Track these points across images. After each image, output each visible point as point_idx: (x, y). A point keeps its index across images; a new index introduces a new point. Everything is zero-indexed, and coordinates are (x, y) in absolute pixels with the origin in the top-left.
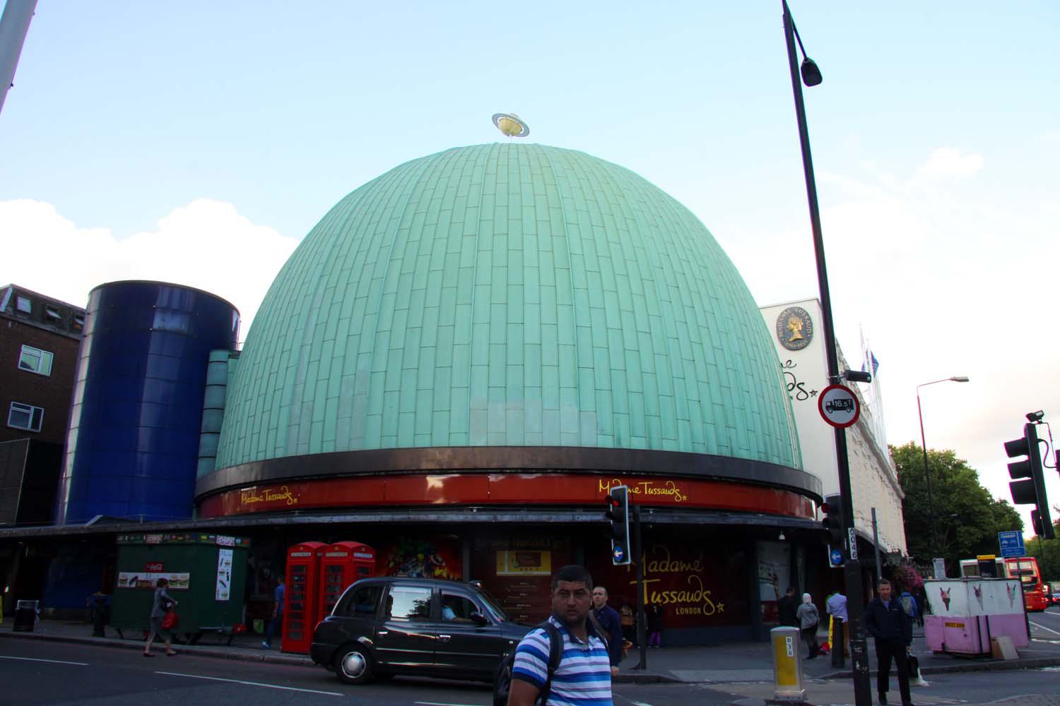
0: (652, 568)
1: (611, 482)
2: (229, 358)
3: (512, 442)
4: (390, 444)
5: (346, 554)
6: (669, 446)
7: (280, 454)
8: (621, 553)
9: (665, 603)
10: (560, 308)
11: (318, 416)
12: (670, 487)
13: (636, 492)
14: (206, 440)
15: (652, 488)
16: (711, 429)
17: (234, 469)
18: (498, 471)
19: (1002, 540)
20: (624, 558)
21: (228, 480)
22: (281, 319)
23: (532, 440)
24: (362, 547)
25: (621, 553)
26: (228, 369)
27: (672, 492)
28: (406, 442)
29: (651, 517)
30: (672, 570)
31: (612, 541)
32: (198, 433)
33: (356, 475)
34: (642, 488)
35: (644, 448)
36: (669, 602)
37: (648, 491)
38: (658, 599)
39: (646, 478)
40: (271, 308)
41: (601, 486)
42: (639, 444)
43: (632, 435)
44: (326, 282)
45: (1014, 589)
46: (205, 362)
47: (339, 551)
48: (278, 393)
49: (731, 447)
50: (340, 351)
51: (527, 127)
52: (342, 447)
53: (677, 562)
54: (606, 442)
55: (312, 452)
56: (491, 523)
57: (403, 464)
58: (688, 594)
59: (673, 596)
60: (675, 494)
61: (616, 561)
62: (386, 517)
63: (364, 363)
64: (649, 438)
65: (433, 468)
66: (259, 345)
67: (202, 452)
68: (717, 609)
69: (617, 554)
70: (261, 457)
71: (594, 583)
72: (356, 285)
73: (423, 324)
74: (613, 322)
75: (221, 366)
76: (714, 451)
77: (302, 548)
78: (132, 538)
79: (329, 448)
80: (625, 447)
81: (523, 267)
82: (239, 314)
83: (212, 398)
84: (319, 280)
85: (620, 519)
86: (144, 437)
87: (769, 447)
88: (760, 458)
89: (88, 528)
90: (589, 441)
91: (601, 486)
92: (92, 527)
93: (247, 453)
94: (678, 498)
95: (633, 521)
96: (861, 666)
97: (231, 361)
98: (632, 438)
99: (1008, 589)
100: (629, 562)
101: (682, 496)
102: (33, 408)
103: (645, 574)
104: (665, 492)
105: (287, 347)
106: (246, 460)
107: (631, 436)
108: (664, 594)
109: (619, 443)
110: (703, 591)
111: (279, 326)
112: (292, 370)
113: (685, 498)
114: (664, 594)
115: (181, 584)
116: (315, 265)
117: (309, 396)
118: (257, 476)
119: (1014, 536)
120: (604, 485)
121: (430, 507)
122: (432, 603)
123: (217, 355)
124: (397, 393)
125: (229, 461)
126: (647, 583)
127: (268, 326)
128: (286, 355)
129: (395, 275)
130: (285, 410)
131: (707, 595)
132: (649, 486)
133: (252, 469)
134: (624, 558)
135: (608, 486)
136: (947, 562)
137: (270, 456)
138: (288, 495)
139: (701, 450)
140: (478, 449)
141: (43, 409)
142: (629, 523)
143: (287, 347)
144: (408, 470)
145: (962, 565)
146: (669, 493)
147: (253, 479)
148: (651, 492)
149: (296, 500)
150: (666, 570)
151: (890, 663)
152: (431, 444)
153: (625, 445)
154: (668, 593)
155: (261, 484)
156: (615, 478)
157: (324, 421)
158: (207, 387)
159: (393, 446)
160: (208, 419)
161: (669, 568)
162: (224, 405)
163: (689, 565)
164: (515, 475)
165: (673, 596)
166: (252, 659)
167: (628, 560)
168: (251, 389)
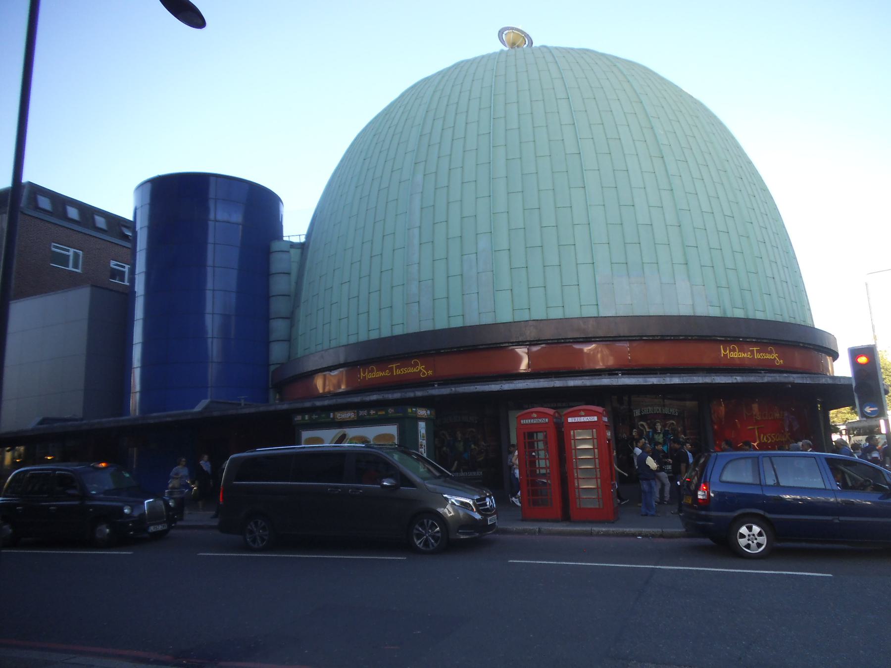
2: (291, 248)
5: (595, 419)
6: (760, 316)
9: (769, 442)
12: (771, 352)
13: (387, 374)
15: (400, 369)
18: (601, 339)
33: (498, 345)
34: (391, 370)
36: (771, 442)
39: (756, 344)
42: (739, 314)
47: (537, 418)
51: (530, 38)
53: (740, 353)
54: (715, 312)
59: (773, 437)
60: (421, 371)
62: (739, 379)
63: (483, 243)
64: (744, 308)
68: (428, 374)
71: (879, 434)
75: (285, 256)
78: (314, 417)
79: (413, 328)
80: (729, 316)
81: (624, 155)
82: (283, 204)
86: (212, 323)
89: (200, 413)
90: (702, 310)
91: (362, 374)
94: (424, 374)
101: (427, 371)
102: (72, 250)
104: (411, 370)
107: (733, 308)
108: (767, 436)
120: (725, 350)
129: (419, 177)
132: (397, 367)
135: (728, 351)
137: (363, 337)
139: (779, 319)
140: (619, 318)
141: (81, 252)
146: (415, 370)
147: (342, 361)
148: (398, 372)
150: (737, 356)
152: (464, 323)
153: (729, 315)
154: (769, 434)
155: (351, 366)
156: (413, 359)
163: (746, 354)
165: (773, 437)
166: (598, 534)
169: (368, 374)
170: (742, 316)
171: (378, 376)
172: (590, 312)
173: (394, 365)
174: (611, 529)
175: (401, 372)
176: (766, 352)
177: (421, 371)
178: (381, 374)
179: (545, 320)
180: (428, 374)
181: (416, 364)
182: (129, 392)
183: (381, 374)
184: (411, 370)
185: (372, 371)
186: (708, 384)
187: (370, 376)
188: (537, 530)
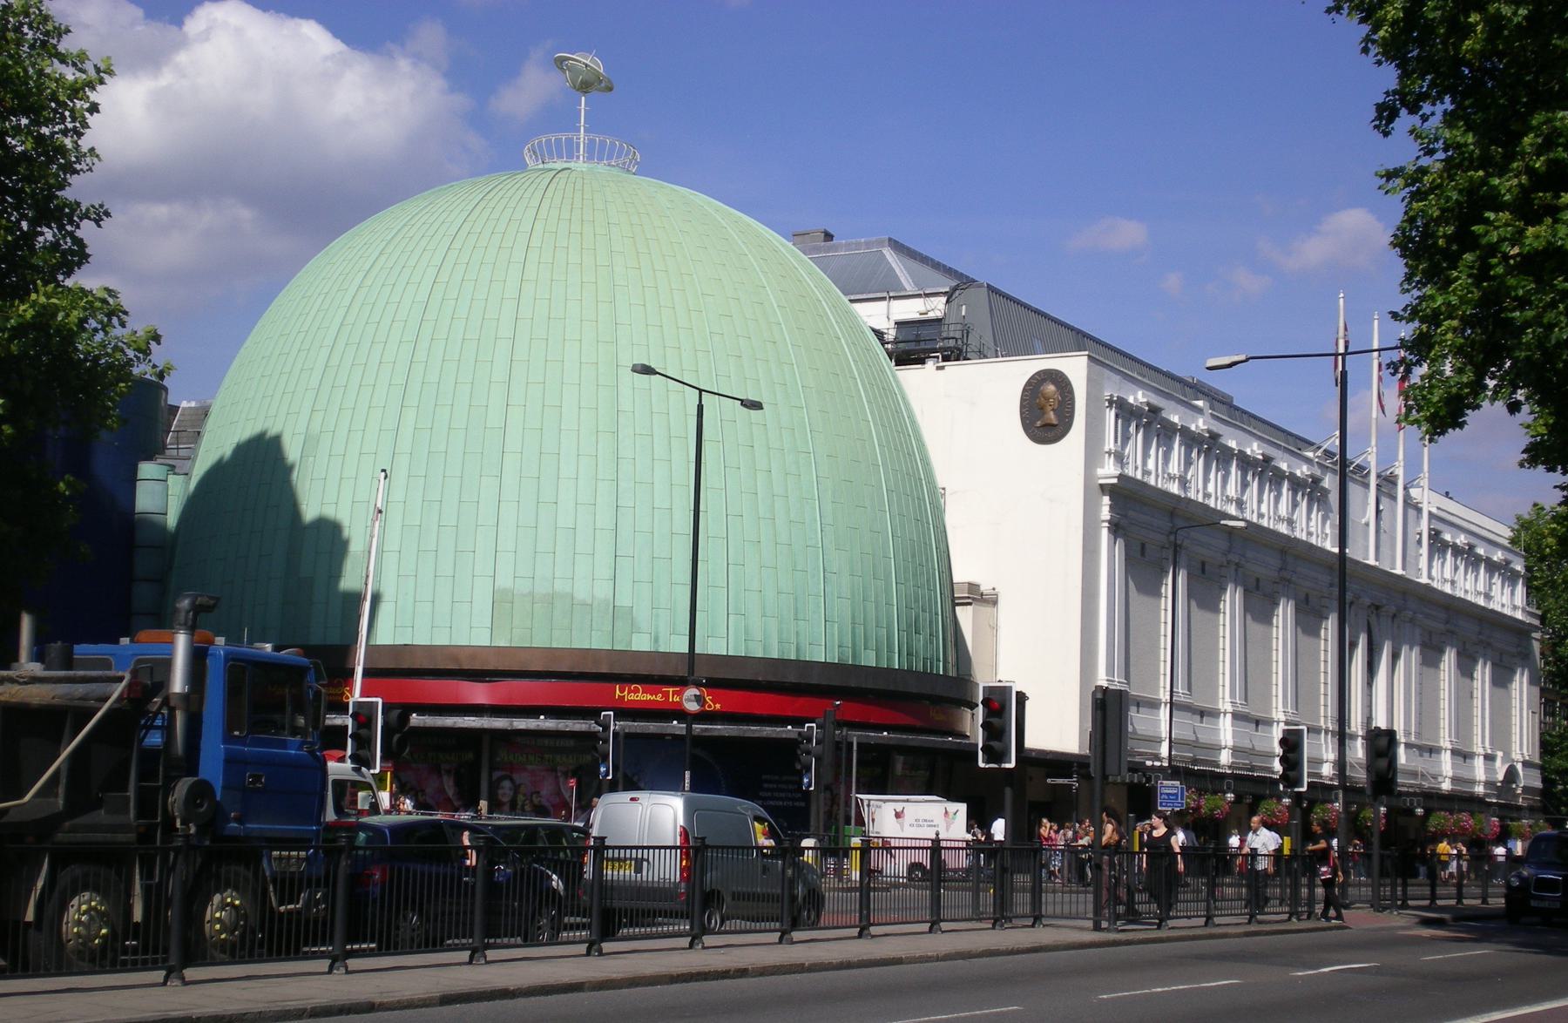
1: (629, 688)
16: (871, 607)
19: (1161, 794)
28: (422, 639)
34: (666, 695)
37: (673, 698)
38: (678, 699)
44: (322, 316)
45: (955, 814)
49: (797, 644)
56: (507, 730)
91: (618, 692)
92: (116, 706)
99: (946, 812)
115: (1510, 177)
116: (311, 313)
119: (1176, 791)
120: (622, 691)
121: (770, 823)
122: (421, 798)
135: (626, 693)
136: (881, 784)
145: (326, 679)
149: (718, 706)
164: (1335, 604)
173: (671, 690)
178: (649, 697)
183: (649, 697)
185: (636, 691)
187: (632, 697)
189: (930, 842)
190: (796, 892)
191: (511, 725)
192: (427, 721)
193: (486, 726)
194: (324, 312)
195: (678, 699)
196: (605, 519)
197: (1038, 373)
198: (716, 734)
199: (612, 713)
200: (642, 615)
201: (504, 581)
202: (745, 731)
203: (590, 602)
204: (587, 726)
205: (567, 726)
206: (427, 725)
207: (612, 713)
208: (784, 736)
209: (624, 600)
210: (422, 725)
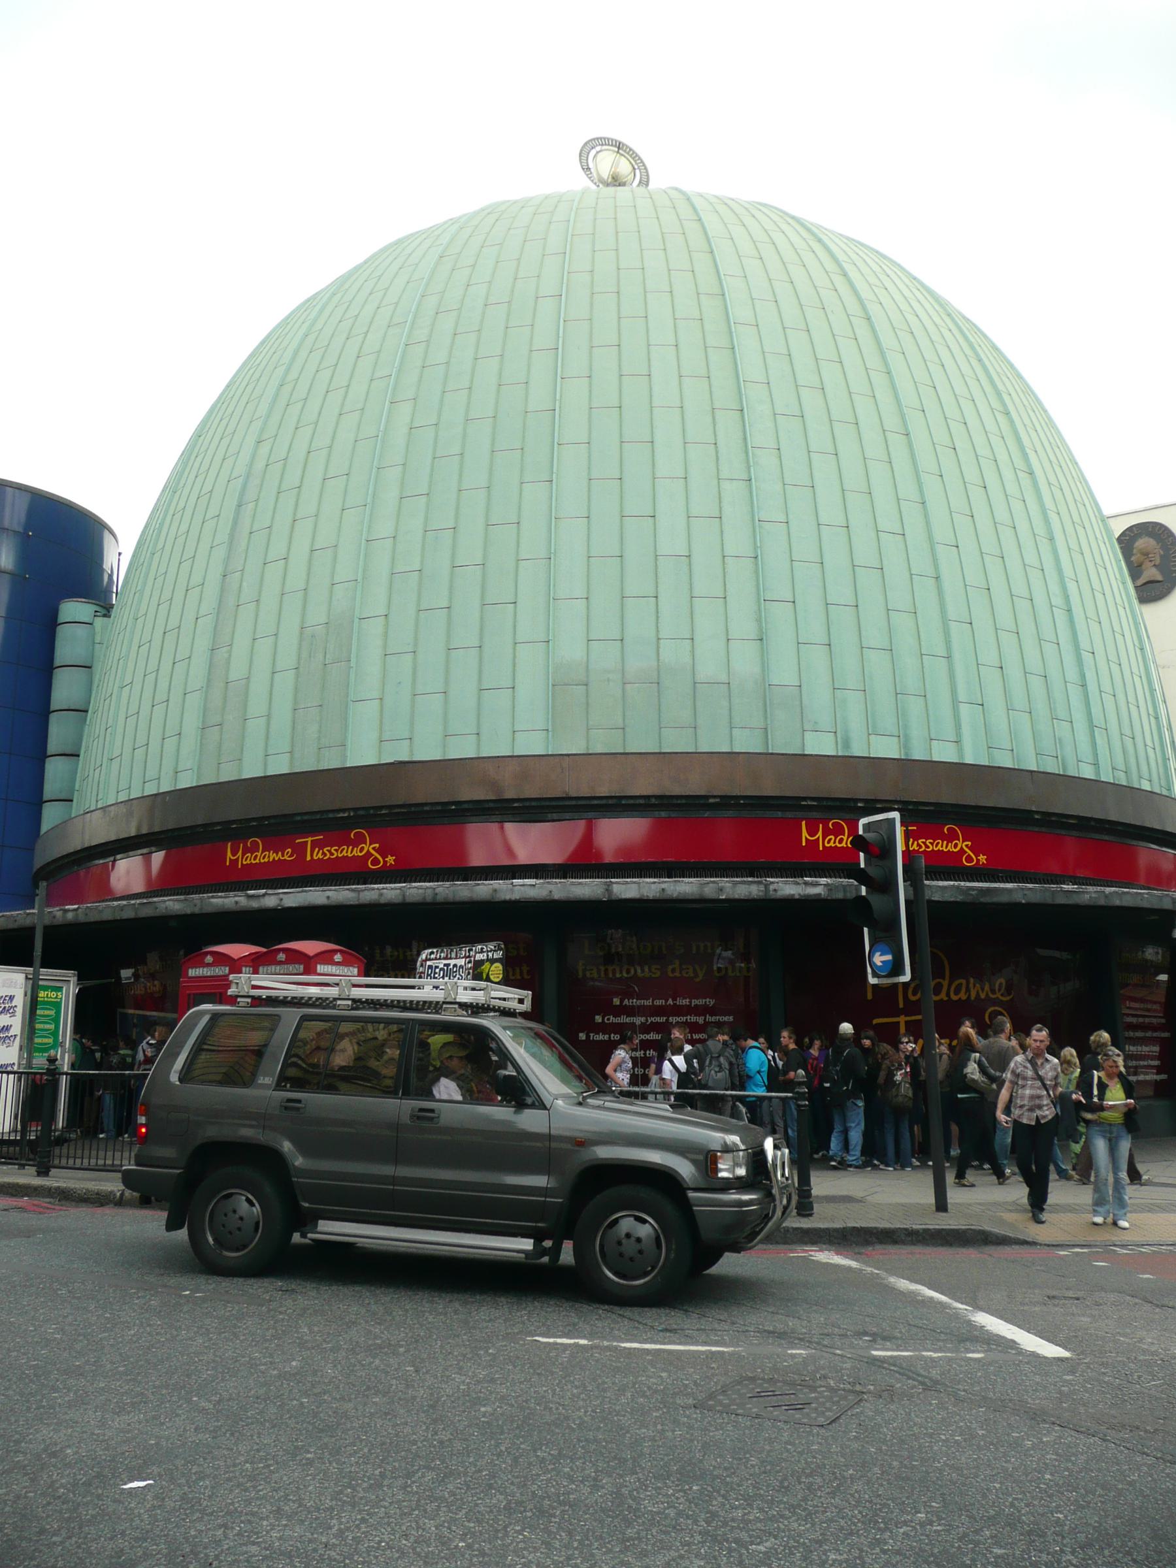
0: (829, 842)
3: (636, 745)
4: (400, 753)
6: (944, 753)
7: (186, 781)
8: (889, 957)
10: (726, 485)
11: (257, 706)
12: (951, 837)
13: (286, 857)
14: (54, 769)
15: (321, 848)
17: (98, 814)
20: (896, 968)
21: (87, 837)
22: (184, 528)
23: (677, 742)
24: (335, 952)
25: (889, 957)
26: (94, 635)
27: (956, 846)
28: (427, 750)
29: (941, 889)
30: (954, 998)
31: (866, 930)
32: (41, 755)
34: (300, 850)
35: (897, 756)
40: (167, 511)
41: (805, 834)
42: (886, 748)
43: (872, 730)
46: (51, 624)
48: (180, 668)
49: (1063, 760)
50: (296, 580)
52: (307, 763)
55: (246, 775)
57: (425, 793)
58: (945, 842)
60: (962, 851)
61: (875, 975)
64: (905, 740)
65: (482, 798)
66: (145, 584)
67: (49, 790)
69: (879, 959)
70: (151, 790)
72: (324, 452)
73: (456, 522)
74: (831, 514)
75: (81, 631)
76: (1031, 764)
77: (209, 959)
79: (280, 766)
83: (64, 689)
84: (279, 390)
85: (886, 886)
87: (1132, 761)
88: (750, 893)
91: (805, 834)
93: (123, 784)
95: (912, 897)
96: (835, 1161)
97: (99, 622)
98: (872, 737)
100: (906, 977)
101: (384, 857)
103: (901, 1006)
104: (347, 852)
105: (196, 579)
106: (122, 797)
109: (847, 744)
110: (370, 844)
111: (181, 540)
112: (206, 623)
113: (983, 858)
114: (920, 841)
117: (237, 672)
118: (139, 827)
120: (812, 832)
123: (73, 610)
124: (409, 657)
125: (93, 802)
126: (906, 1022)
127: (160, 546)
128: (194, 594)
130: (194, 700)
131: (967, 846)
133: (130, 814)
134: (896, 968)
135: (820, 834)
138: (369, 847)
139: (1005, 761)
142: (907, 902)
143: (196, 579)
144: (432, 804)
146: (951, 848)
149: (983, 858)
151: (1049, 1170)
153: (858, 750)
157: (269, 716)
158: (48, 760)
159: (404, 757)
160: (58, 733)
161: (948, 995)
162: (72, 790)
167: (903, 973)
168: (131, 665)
169: (243, 855)
170: (894, 754)
171: (266, 860)
172: (746, 742)
173: (309, 839)
174: (869, 1269)
175: (325, 855)
176: (937, 835)
177: (369, 854)
178: (273, 856)
179: (583, 754)
180: (385, 862)
181: (360, 840)
182: (702, 900)
183: (273, 856)
184: (347, 852)
185: (254, 849)
186: (754, 901)
187: (249, 859)
188: (118, 1194)
189: (318, 971)
190: (430, 958)
191: (608, 890)
192: (438, 890)
193: (557, 895)
194: (300, 405)
195: (320, 856)
196: (738, 542)
197: (1130, 529)
198: (1004, 899)
199: (895, 815)
200: (819, 698)
201: (571, 650)
202: (1054, 893)
203: (723, 678)
204: (762, 888)
205: (721, 890)
206: (440, 899)
207: (895, 815)
208: (1117, 903)
209: (784, 674)
210: (429, 899)
